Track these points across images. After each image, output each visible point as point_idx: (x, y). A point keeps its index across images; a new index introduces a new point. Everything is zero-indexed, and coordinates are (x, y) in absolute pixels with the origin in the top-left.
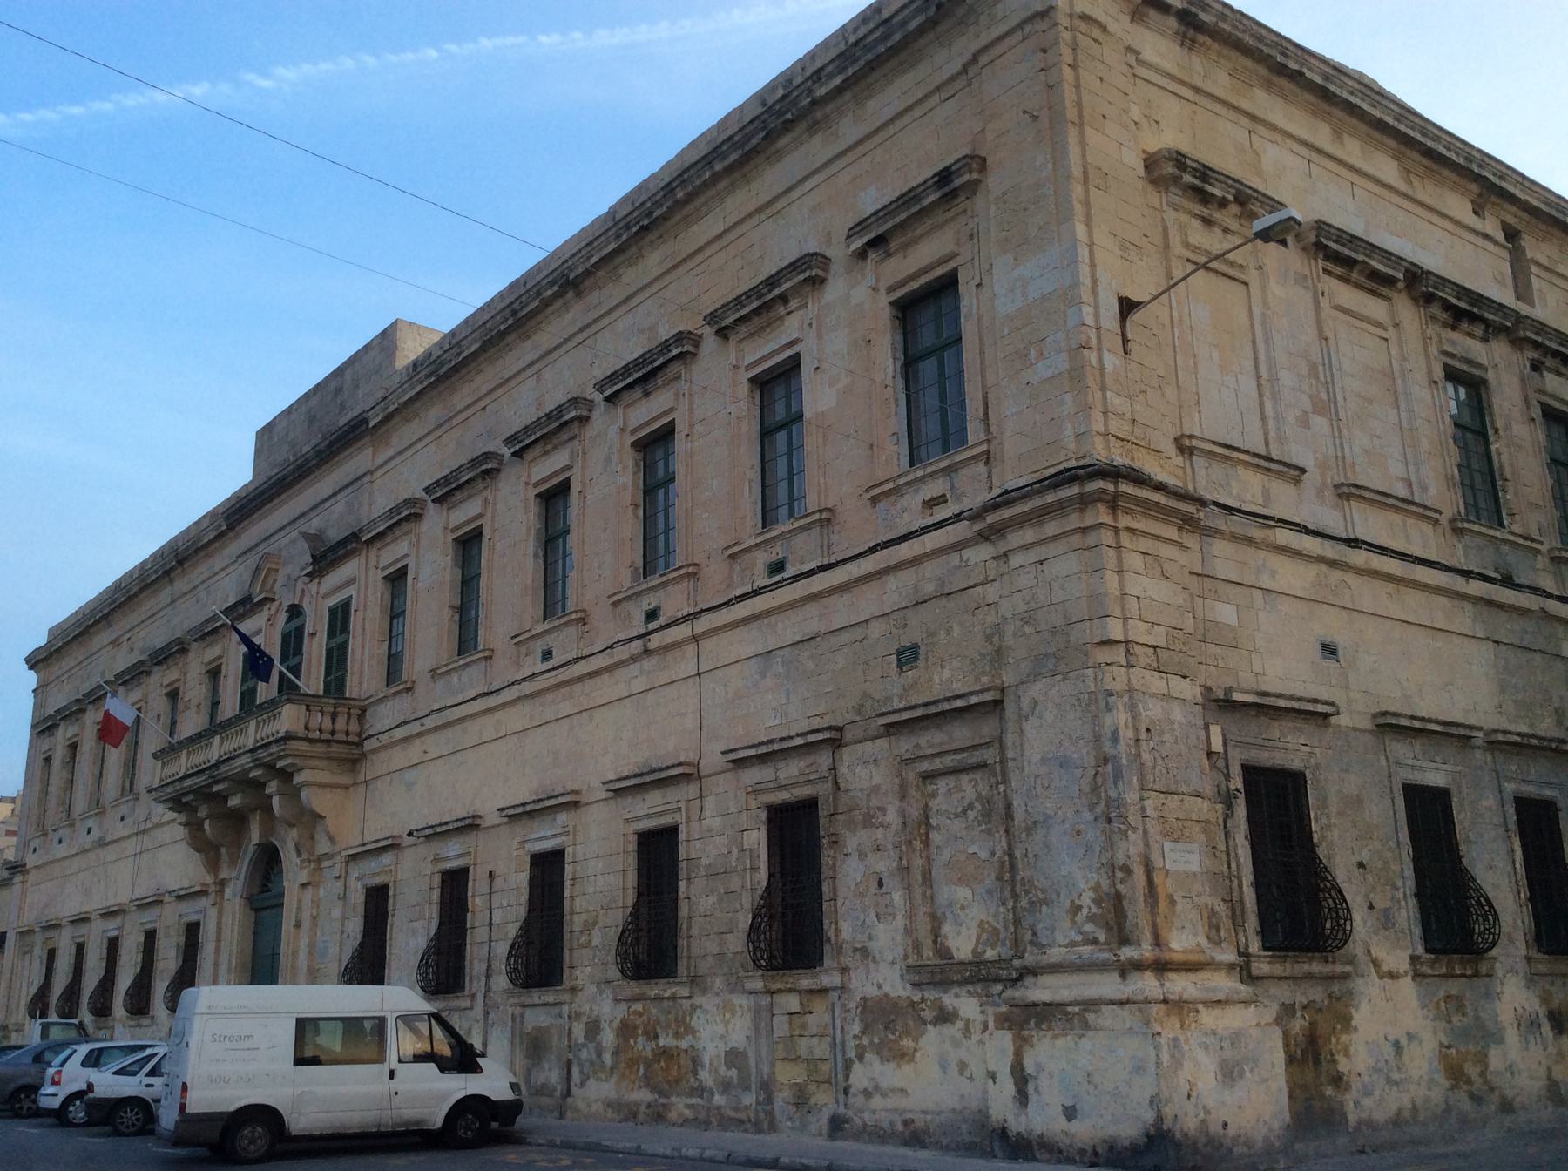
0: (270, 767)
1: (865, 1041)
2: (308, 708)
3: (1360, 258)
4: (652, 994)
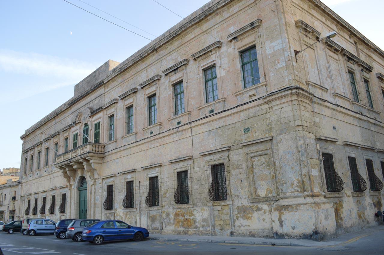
0: (84, 159)
1: (239, 215)
2: (93, 146)
3: (333, 46)
4: (183, 207)
